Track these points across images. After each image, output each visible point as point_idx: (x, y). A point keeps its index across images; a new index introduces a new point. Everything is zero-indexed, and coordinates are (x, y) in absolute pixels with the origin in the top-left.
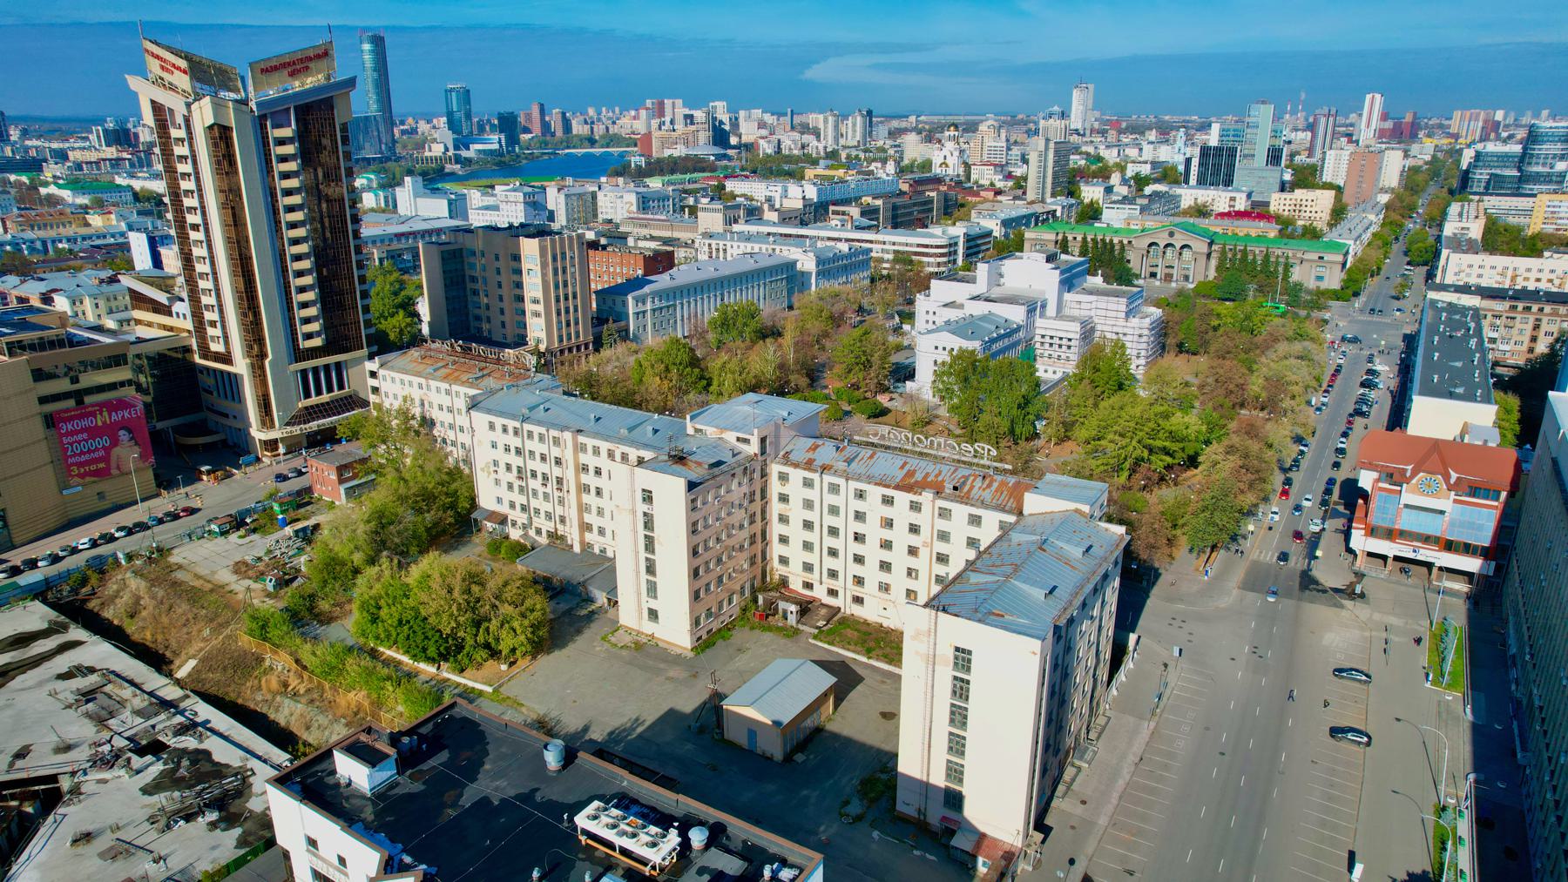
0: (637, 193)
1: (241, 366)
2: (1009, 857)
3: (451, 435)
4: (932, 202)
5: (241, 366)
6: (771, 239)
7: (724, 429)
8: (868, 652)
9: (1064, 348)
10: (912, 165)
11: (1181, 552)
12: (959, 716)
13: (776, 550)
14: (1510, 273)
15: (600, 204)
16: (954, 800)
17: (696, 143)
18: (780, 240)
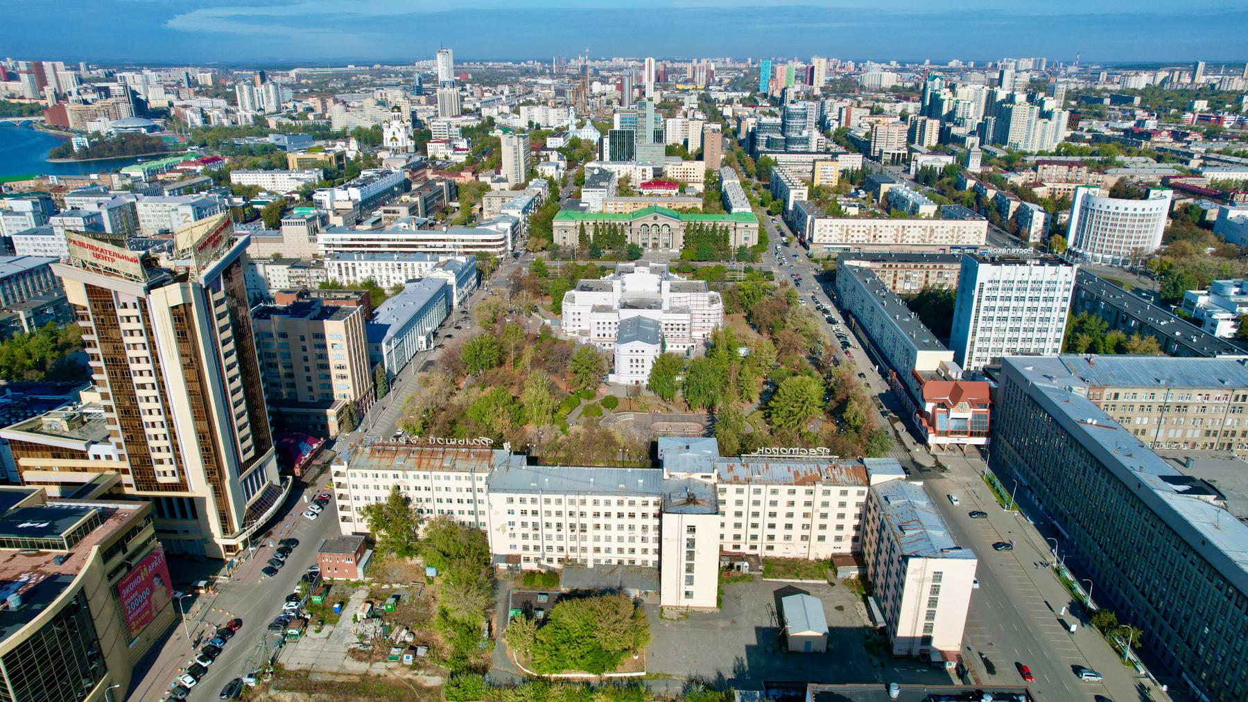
0: (193, 205)
1: (199, 487)
2: (959, 658)
4: (442, 191)
5: (199, 487)
6: (396, 256)
8: (797, 576)
9: (675, 330)
10: (345, 130)
12: (933, 603)
14: (845, 228)
15: (140, 213)
16: (927, 640)
17: (118, 118)
18: (402, 256)
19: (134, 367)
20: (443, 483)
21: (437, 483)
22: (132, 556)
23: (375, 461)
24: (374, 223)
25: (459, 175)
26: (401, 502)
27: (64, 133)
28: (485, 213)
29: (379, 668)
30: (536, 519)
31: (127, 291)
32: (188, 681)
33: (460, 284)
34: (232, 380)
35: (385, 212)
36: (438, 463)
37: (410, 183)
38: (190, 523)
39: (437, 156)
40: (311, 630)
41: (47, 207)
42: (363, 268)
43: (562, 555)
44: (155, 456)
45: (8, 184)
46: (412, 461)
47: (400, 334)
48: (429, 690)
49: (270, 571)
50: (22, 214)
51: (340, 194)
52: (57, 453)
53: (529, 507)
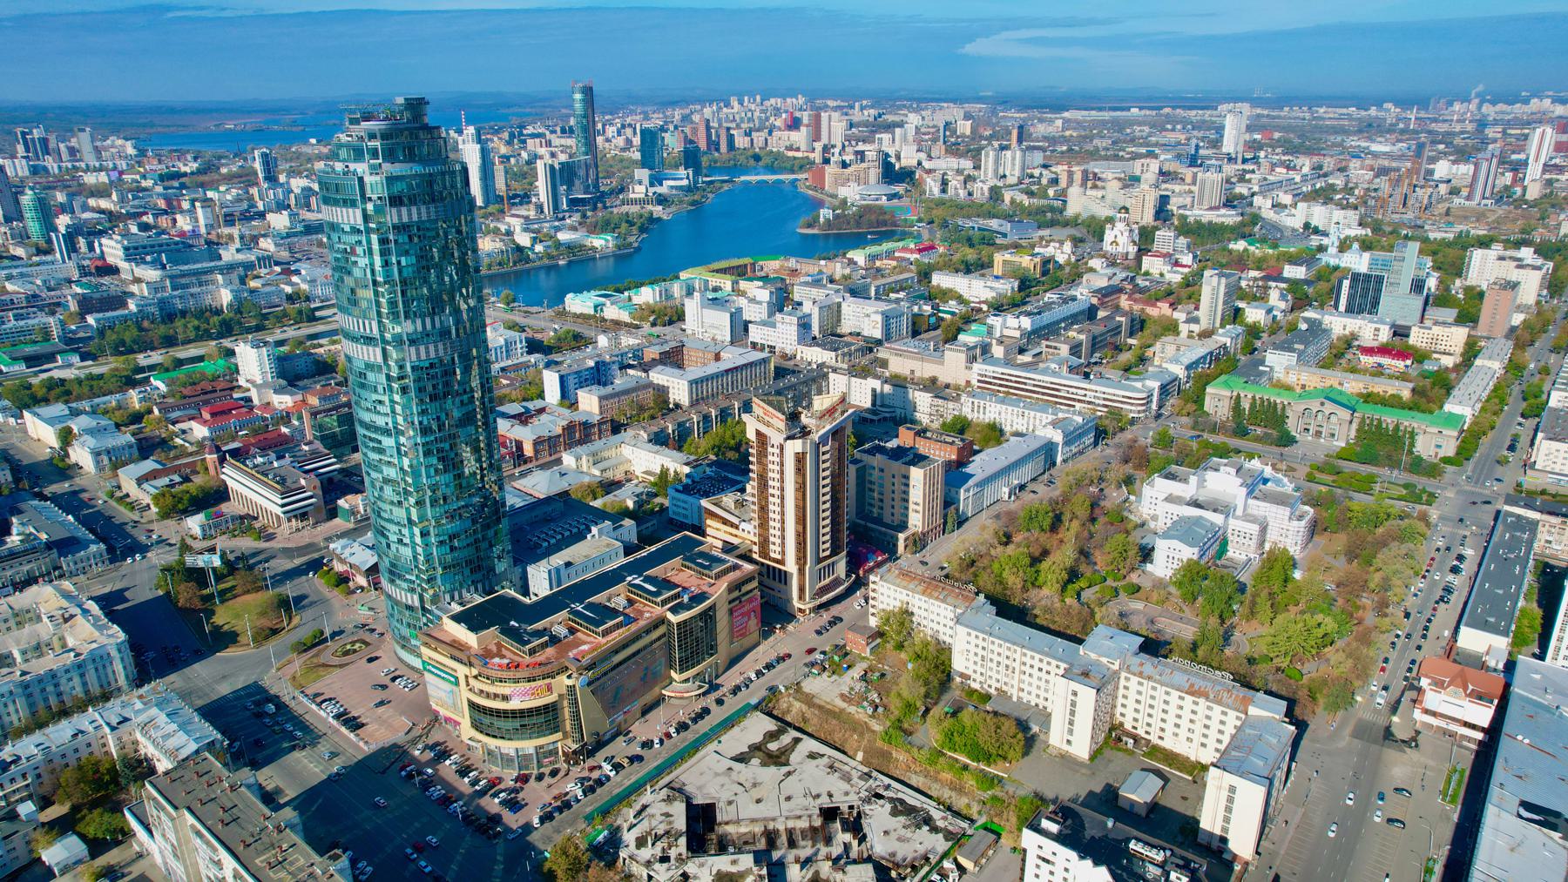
1: (791, 566)
2: (1247, 863)
3: (924, 622)
4: (1120, 326)
7: (1100, 656)
8: (1170, 766)
10: (1077, 216)
11: (1319, 710)
12: (1229, 809)
13: (1119, 710)
16: (1224, 840)
19: (770, 483)
20: (936, 610)
21: (932, 608)
22: (744, 595)
23: (898, 581)
24: (1035, 356)
25: (1154, 305)
26: (906, 614)
27: (820, 196)
28: (1156, 359)
29: (852, 709)
30: (985, 653)
31: (776, 438)
32: (753, 676)
33: (1067, 443)
34: (824, 503)
35: (1047, 347)
36: (936, 594)
37: (1097, 309)
38: (782, 586)
39: (1151, 271)
40: (826, 673)
41: (782, 300)
42: (993, 409)
43: (998, 686)
44: (772, 539)
45: (761, 263)
46: (920, 588)
47: (982, 484)
48: (873, 731)
49: (819, 633)
50: (760, 303)
51: (1011, 321)
52: (725, 522)
53: (982, 644)
